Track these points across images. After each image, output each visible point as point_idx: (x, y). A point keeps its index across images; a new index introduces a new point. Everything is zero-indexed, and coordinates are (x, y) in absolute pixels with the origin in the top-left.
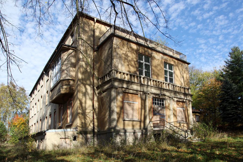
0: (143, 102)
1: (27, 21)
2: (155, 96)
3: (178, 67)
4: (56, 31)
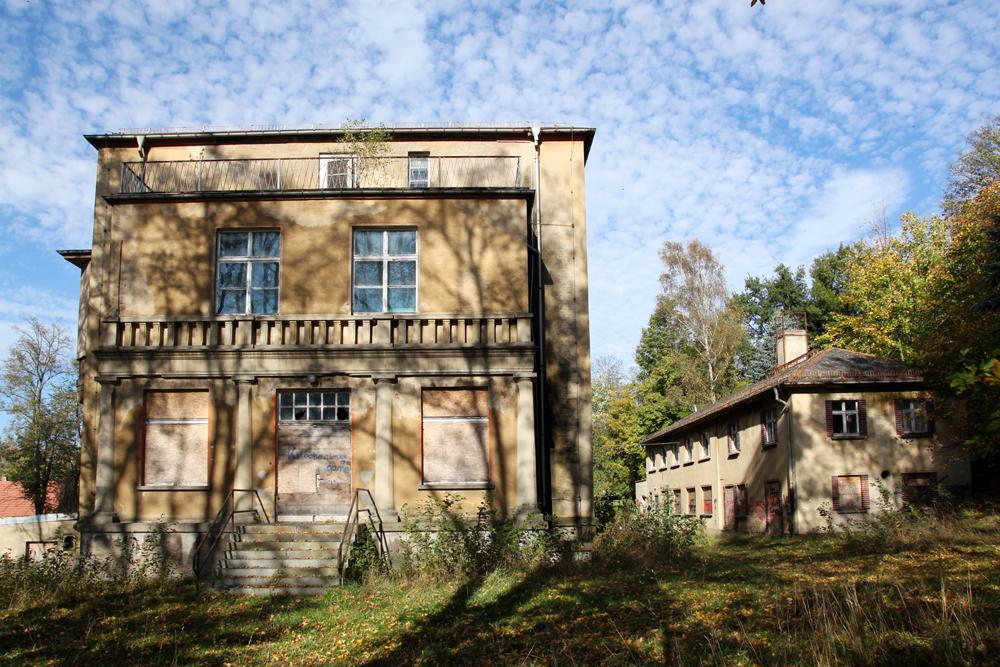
0: (224, 416)
1: (452, 41)
2: (289, 383)
3: (443, 230)
4: (561, 43)
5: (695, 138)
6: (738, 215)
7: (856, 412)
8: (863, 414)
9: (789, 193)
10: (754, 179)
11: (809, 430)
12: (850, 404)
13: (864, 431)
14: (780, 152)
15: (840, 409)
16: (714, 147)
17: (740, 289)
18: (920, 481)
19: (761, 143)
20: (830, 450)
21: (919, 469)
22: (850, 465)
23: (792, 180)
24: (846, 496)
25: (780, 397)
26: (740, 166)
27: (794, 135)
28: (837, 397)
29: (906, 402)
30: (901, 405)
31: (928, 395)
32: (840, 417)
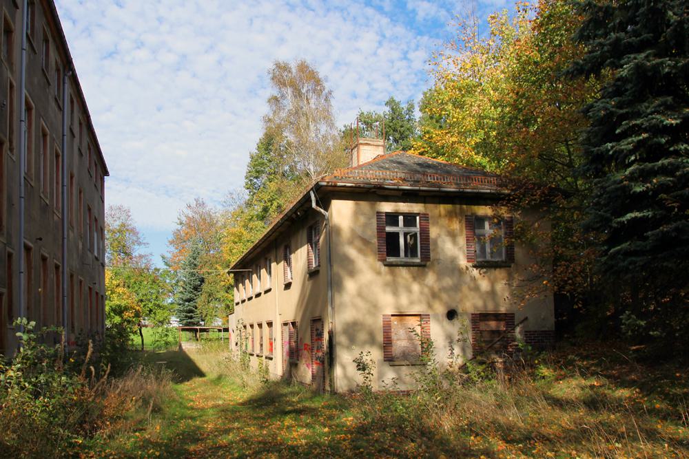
5: (328, 10)
6: (369, 83)
7: (417, 229)
8: (425, 232)
9: (410, 67)
10: (381, 51)
11: (352, 252)
12: (410, 219)
13: (426, 257)
14: (400, 30)
15: (397, 224)
16: (345, 19)
17: (343, 129)
18: (493, 324)
19: (385, 21)
20: (379, 281)
21: (490, 308)
22: (404, 300)
23: (411, 55)
24: (400, 343)
25: (317, 204)
26: (368, 40)
27: (411, 15)
28: (387, 207)
29: (480, 221)
30: (474, 223)
31: (504, 212)
32: (396, 235)
